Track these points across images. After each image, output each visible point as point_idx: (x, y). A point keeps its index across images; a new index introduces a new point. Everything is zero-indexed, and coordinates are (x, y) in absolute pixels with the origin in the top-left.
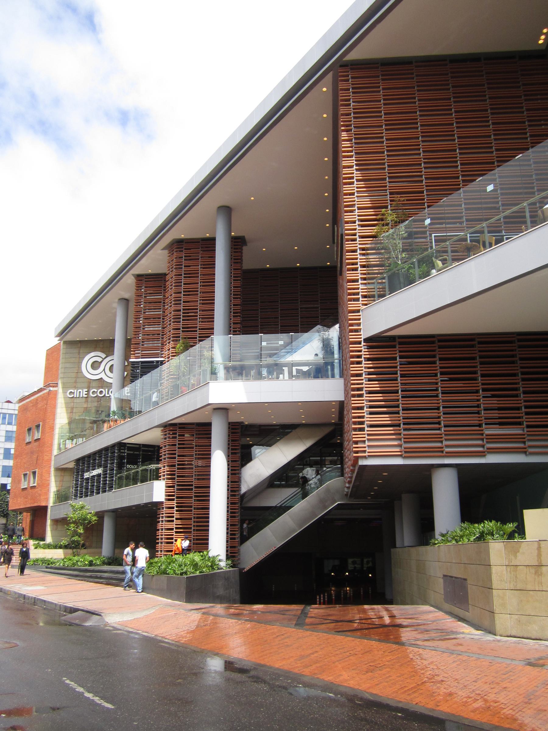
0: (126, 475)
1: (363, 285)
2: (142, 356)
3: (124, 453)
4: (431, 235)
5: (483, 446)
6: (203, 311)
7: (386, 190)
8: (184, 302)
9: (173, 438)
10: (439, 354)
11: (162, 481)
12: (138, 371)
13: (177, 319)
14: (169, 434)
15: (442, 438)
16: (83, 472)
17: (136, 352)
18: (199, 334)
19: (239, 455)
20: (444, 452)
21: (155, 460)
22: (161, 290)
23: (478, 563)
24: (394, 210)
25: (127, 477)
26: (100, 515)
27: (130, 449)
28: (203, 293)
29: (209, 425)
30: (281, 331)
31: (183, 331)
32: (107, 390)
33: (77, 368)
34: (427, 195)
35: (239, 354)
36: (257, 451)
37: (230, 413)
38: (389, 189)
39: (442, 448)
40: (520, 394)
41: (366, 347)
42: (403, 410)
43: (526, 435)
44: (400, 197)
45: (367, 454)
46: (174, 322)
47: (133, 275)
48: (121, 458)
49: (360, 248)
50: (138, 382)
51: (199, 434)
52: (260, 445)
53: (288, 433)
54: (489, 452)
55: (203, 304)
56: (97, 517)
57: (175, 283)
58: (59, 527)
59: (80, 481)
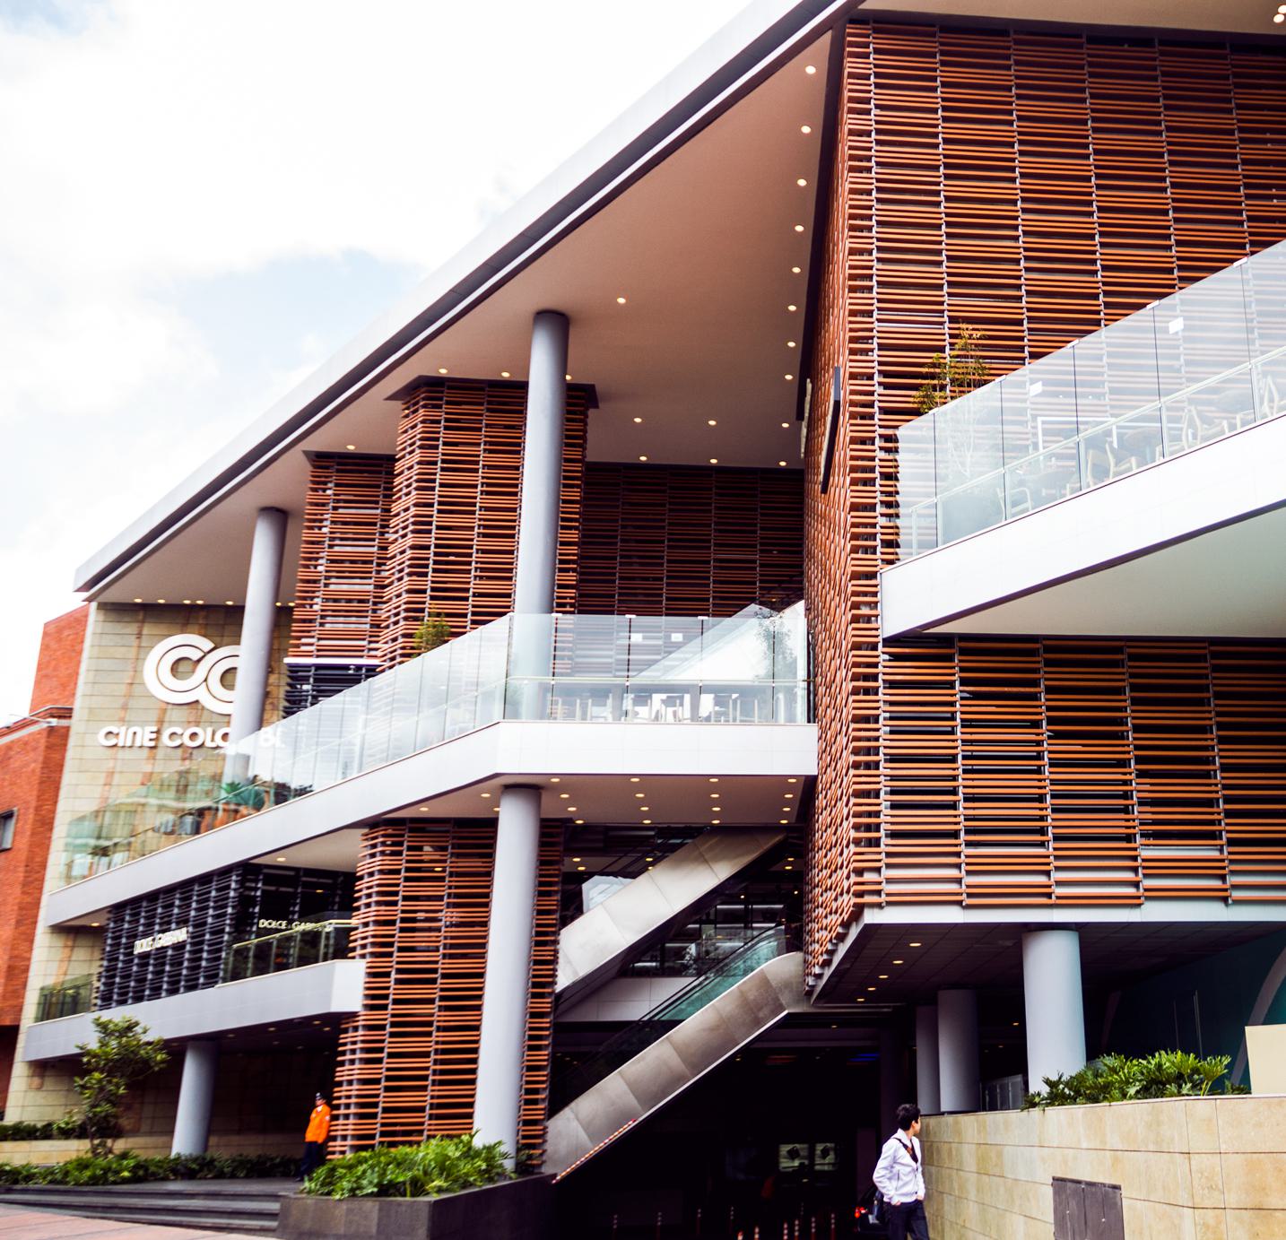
0: (258, 946)
1: (884, 518)
2: (318, 650)
3: (256, 889)
4: (1034, 417)
5: (1136, 885)
6: (484, 552)
7: (943, 311)
8: (438, 528)
9: (393, 853)
10: (1046, 679)
11: (357, 960)
12: (305, 687)
13: (418, 569)
14: (383, 844)
15: (1048, 864)
16: (134, 936)
17: (304, 641)
18: (474, 606)
19: (558, 897)
20: (1053, 896)
21: (336, 907)
22: (378, 496)
23: (1151, 1148)
24: (958, 356)
25: (263, 950)
26: (176, 1049)
27: (268, 880)
28: (487, 509)
29: (492, 824)
30: (667, 609)
31: (432, 598)
32: (210, 730)
33: (132, 673)
34: (1029, 329)
35: (570, 658)
36: (597, 891)
37: (545, 797)
38: (949, 311)
39: (1050, 886)
40: (1215, 771)
41: (887, 657)
42: (966, 800)
43: (1052, 858)
44: (973, 329)
45: (883, 898)
46: (410, 574)
47: (306, 453)
48: (244, 902)
49: (881, 436)
50: (304, 716)
51: (460, 846)
52: (608, 874)
53: (674, 849)
54: (1148, 898)
55: (485, 535)
56: (167, 1053)
57: (417, 481)
58: (50, 1083)
59: (123, 962)
